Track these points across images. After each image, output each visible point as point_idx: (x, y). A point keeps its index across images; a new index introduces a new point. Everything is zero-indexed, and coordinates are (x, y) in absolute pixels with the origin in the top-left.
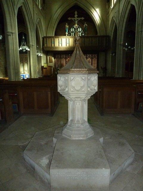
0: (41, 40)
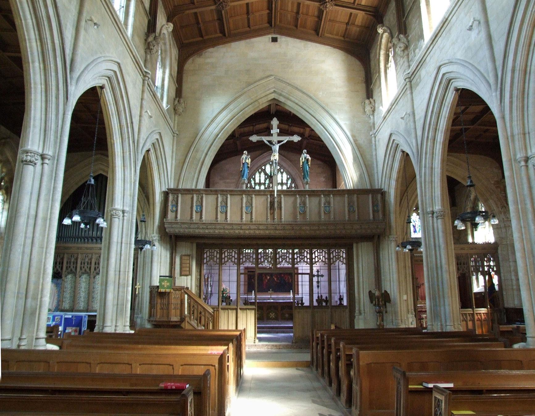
0: (158, 198)
